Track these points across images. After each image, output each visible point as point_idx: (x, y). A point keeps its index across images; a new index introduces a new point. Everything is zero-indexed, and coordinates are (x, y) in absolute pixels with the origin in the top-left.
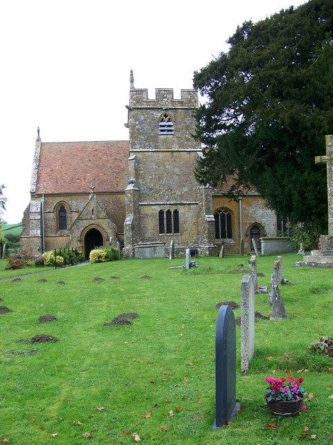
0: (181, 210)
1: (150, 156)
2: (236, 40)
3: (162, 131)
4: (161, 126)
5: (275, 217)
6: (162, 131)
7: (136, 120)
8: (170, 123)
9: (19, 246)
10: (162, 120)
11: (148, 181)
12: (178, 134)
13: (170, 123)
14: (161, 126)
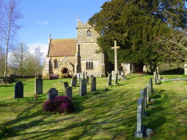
0: (94, 62)
1: (84, 44)
2: (104, 6)
3: (87, 35)
4: (87, 34)
5: (168, 70)
6: (87, 35)
7: (79, 32)
8: (90, 33)
9: (10, 57)
10: (88, 32)
11: (83, 52)
12: (93, 36)
13: (90, 33)
14: (87, 34)
